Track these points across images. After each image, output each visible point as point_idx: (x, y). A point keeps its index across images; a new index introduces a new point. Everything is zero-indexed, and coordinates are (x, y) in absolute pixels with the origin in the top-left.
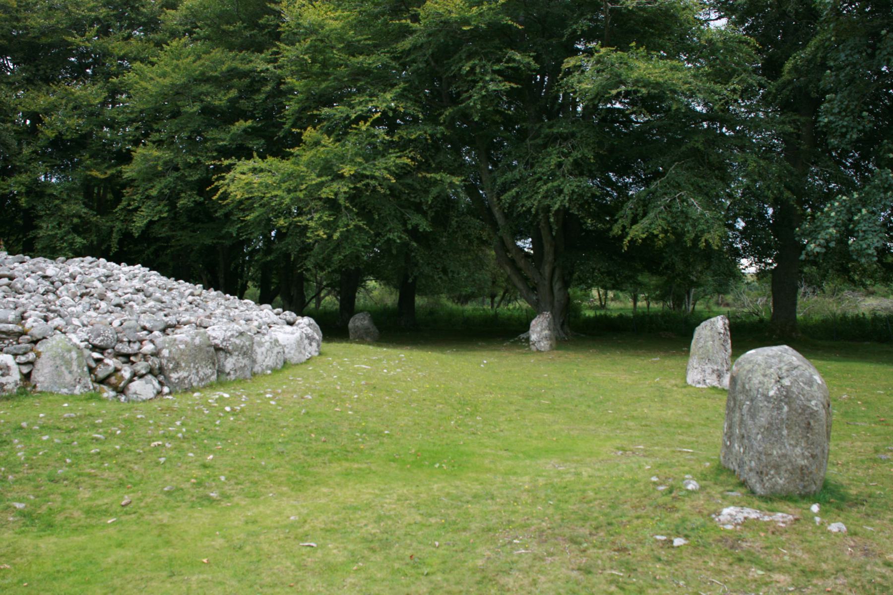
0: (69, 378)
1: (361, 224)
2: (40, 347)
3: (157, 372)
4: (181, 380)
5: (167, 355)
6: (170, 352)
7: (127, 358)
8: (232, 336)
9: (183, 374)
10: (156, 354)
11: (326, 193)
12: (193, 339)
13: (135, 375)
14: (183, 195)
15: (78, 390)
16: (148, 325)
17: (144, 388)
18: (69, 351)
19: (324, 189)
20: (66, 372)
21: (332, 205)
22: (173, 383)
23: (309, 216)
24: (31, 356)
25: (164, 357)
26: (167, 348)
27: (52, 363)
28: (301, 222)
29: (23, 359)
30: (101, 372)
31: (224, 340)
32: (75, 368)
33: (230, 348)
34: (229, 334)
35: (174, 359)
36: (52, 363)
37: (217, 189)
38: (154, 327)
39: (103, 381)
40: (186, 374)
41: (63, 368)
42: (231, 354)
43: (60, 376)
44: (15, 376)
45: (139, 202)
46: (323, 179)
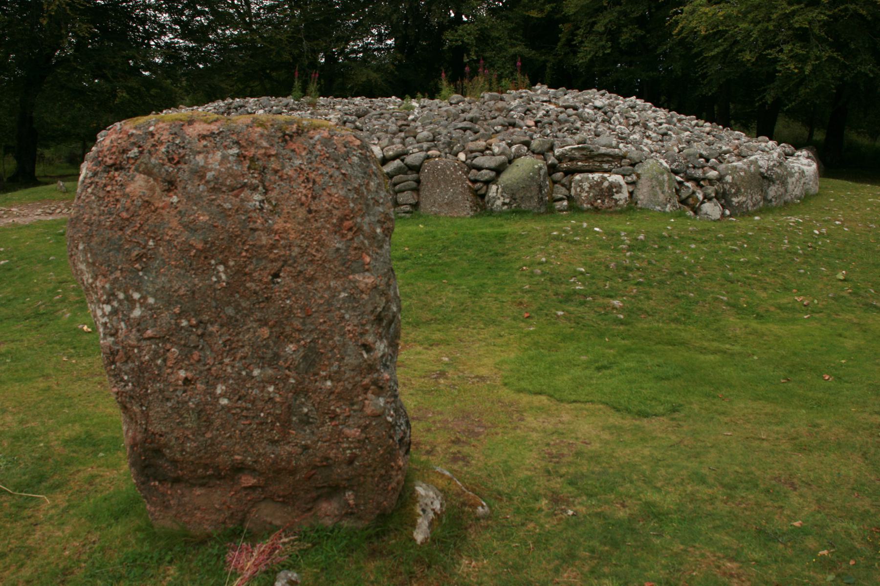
0: (661, 197)
1: (835, 55)
2: (639, 170)
3: (723, 198)
4: (740, 204)
5: (730, 181)
6: (733, 178)
7: (697, 181)
8: (774, 165)
9: (742, 199)
10: (720, 179)
11: (799, 22)
12: (749, 167)
13: (707, 198)
14: (625, 30)
15: (668, 208)
16: (704, 153)
17: (712, 209)
18: (662, 174)
19: (796, 18)
20: (660, 192)
21: (803, 36)
22: (734, 206)
23: (778, 48)
24: (634, 177)
25: (727, 183)
26: (730, 174)
27: (649, 183)
28: (771, 55)
29: (629, 179)
30: (684, 194)
31: (768, 169)
32: (666, 189)
33: (774, 177)
34: (772, 164)
35: (736, 185)
36: (649, 183)
37: (677, 23)
38: (710, 154)
39: (683, 202)
40: (744, 199)
41: (658, 188)
42: (774, 183)
43: (655, 195)
44: (624, 194)
45: (582, 36)
46: (795, 7)
